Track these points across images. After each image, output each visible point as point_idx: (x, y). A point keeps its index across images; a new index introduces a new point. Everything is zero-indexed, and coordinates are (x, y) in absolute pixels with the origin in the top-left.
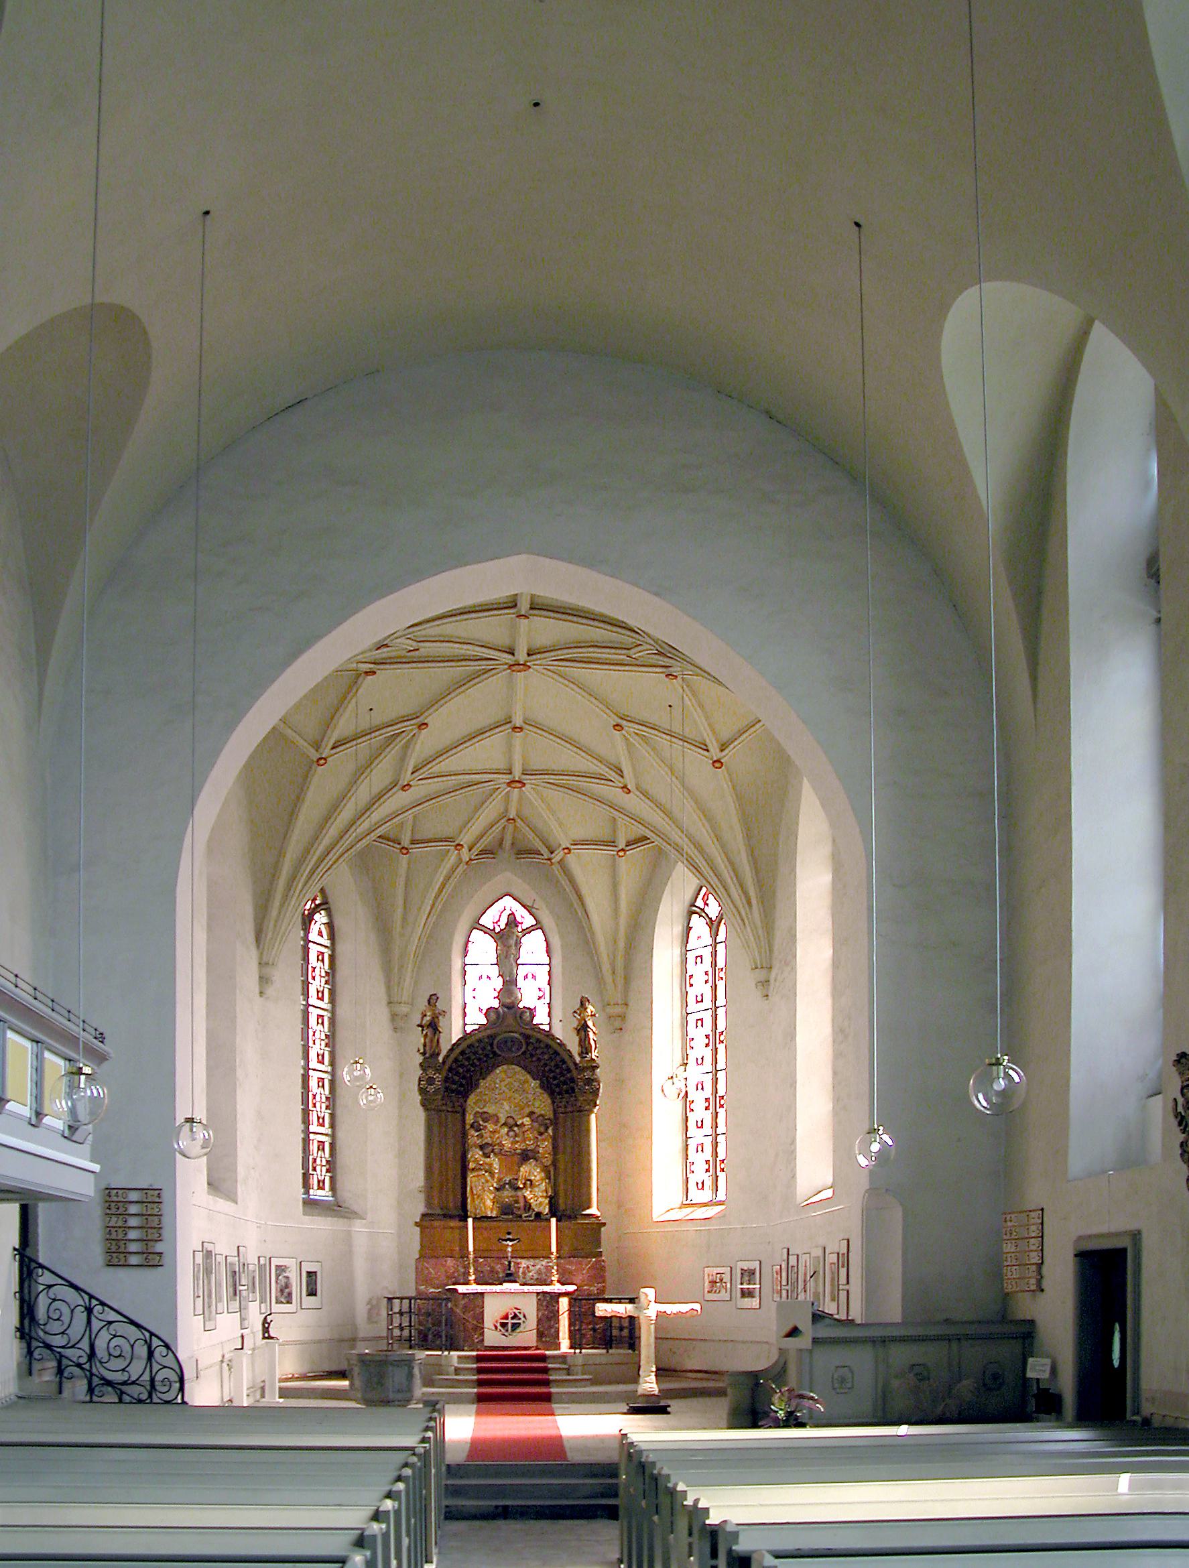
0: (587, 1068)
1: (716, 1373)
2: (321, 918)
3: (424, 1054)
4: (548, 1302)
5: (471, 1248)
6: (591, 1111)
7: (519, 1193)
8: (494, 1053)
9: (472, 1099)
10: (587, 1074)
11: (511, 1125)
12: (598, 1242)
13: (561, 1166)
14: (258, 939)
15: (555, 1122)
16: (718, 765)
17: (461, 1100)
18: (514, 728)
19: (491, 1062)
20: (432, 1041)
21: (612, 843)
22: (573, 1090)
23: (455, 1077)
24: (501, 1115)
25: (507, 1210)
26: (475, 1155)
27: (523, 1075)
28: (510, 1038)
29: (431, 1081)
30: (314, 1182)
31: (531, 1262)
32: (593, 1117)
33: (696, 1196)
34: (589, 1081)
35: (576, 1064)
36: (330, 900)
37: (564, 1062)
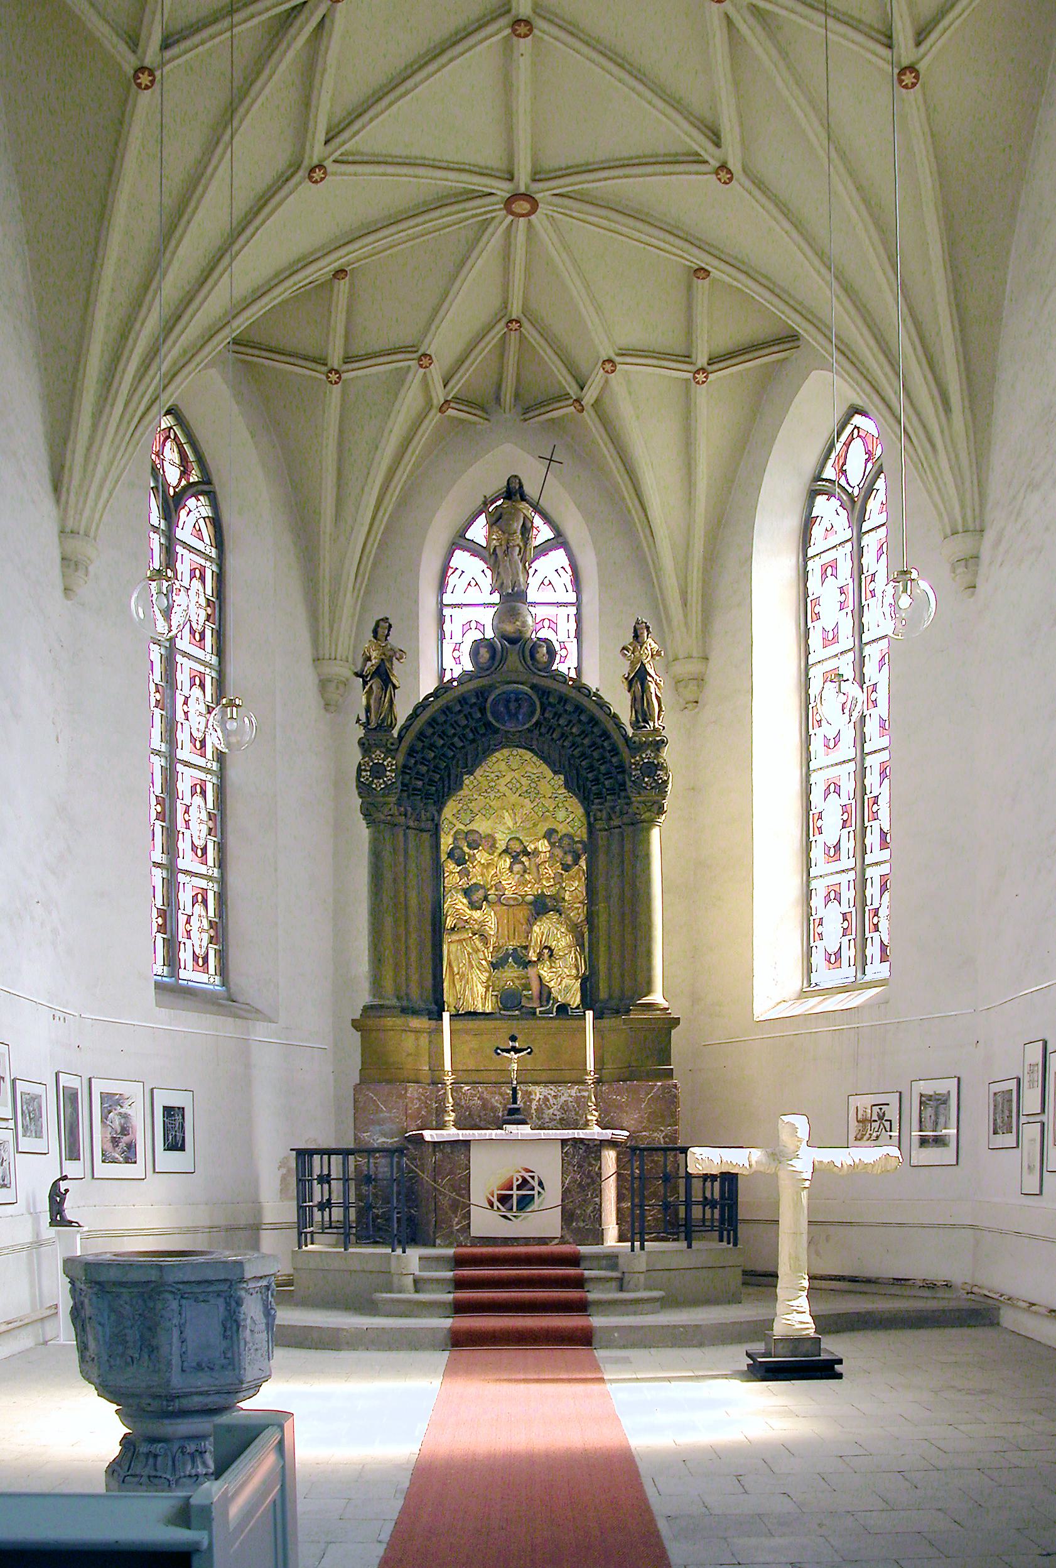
1: (869, 1281)
2: (196, 509)
3: (366, 725)
4: (582, 1157)
5: (448, 1066)
6: (652, 822)
7: (531, 972)
8: (488, 725)
9: (450, 809)
10: (647, 755)
11: (518, 854)
12: (664, 1053)
13: (602, 921)
14: (57, 486)
15: (590, 847)
16: (908, 79)
17: (433, 809)
18: (518, 22)
20: (380, 701)
21: (686, 357)
23: (418, 763)
24: (498, 836)
26: (456, 905)
28: (516, 702)
29: (378, 771)
30: (185, 956)
31: (550, 1091)
32: (655, 833)
33: (825, 976)
34: (653, 768)
35: (625, 736)
36: (215, 479)
37: (606, 735)
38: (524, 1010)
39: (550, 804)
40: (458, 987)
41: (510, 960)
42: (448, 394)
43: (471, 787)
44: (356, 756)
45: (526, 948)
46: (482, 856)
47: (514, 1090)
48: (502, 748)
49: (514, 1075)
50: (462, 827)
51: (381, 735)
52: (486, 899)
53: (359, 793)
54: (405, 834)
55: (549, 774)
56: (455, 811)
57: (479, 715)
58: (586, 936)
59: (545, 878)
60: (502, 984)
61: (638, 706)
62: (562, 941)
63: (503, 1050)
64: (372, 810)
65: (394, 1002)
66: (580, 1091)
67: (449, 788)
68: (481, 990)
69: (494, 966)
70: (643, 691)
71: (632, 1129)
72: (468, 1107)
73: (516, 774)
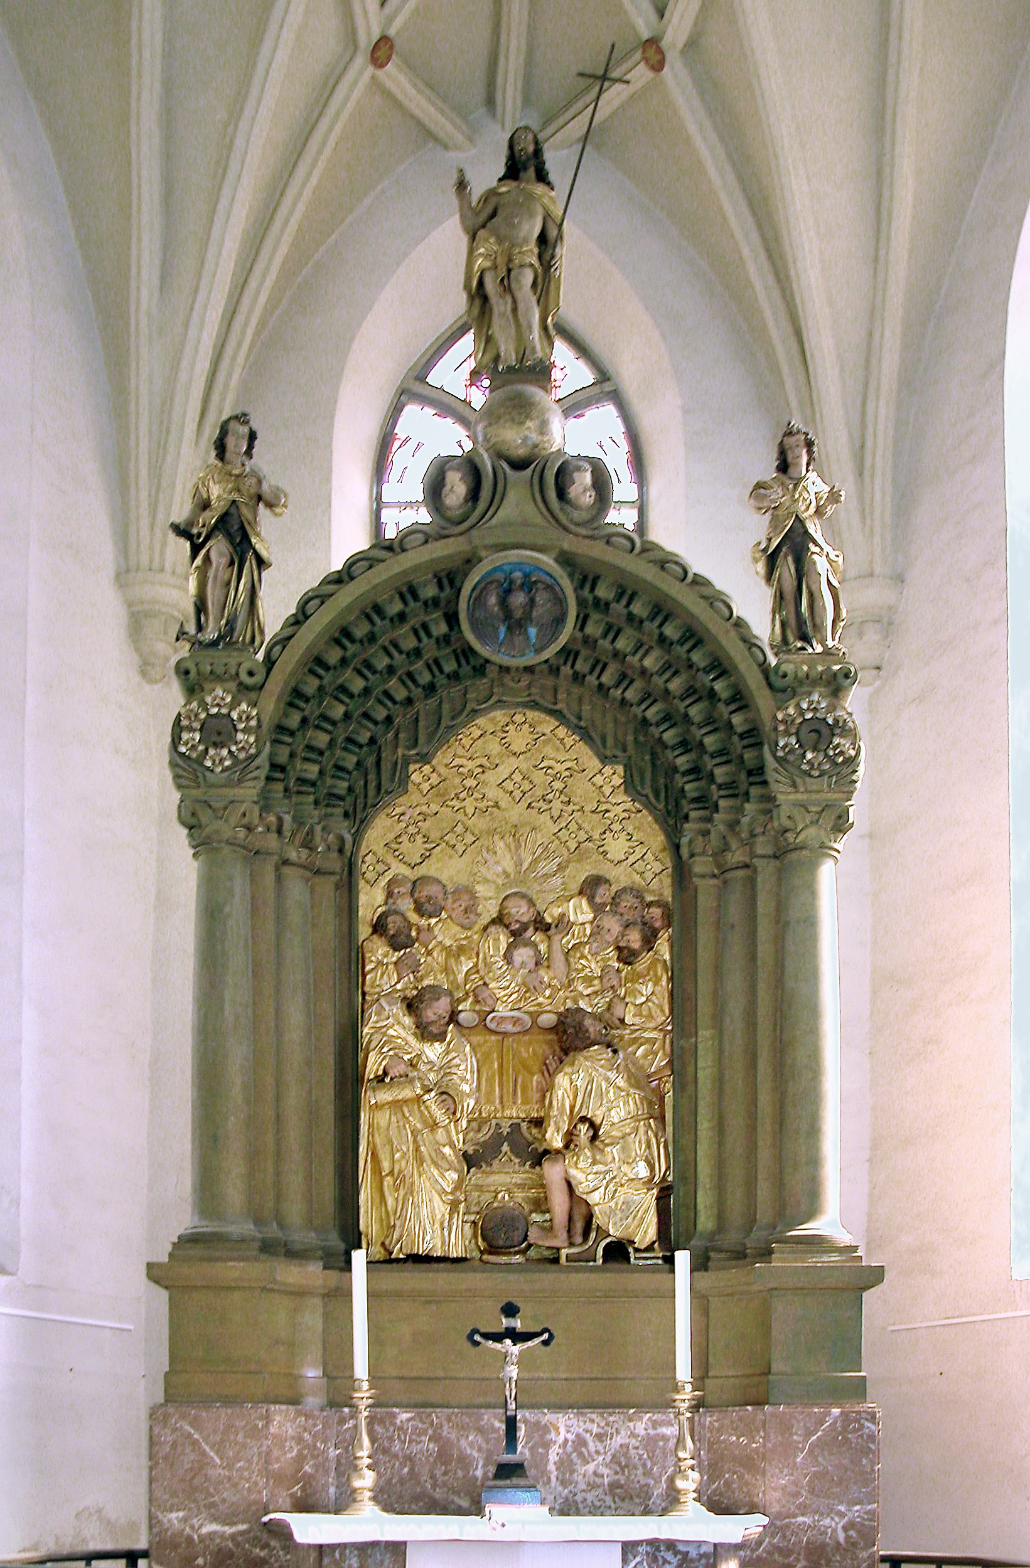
0: (810, 681)
5: (361, 1369)
7: (553, 1172)
8: (467, 652)
9: (379, 832)
12: (847, 1346)
15: (680, 914)
17: (344, 829)
19: (450, 693)
22: (757, 772)
24: (481, 890)
25: (498, 1235)
26: (389, 1031)
27: (565, 751)
29: (218, 731)
32: (826, 873)
34: (823, 733)
35: (763, 666)
38: (532, 1253)
39: (593, 825)
40: (390, 1202)
41: (505, 1148)
42: (390, 20)
43: (426, 787)
44: (172, 698)
45: (539, 1123)
46: (445, 932)
47: (511, 1424)
48: (492, 708)
49: (511, 1391)
50: (404, 870)
51: (222, 658)
52: (453, 1018)
53: (177, 777)
54: (279, 879)
55: (594, 763)
56: (392, 836)
57: (443, 628)
58: (669, 1098)
59: (581, 976)
60: (487, 1197)
61: (789, 612)
62: (618, 1108)
63: (487, 1336)
64: (205, 816)
65: (247, 1228)
66: (655, 1424)
67: (379, 787)
68: (442, 1209)
69: (471, 1160)
70: (800, 575)
71: (775, 1508)
72: (409, 1458)
73: (523, 763)
